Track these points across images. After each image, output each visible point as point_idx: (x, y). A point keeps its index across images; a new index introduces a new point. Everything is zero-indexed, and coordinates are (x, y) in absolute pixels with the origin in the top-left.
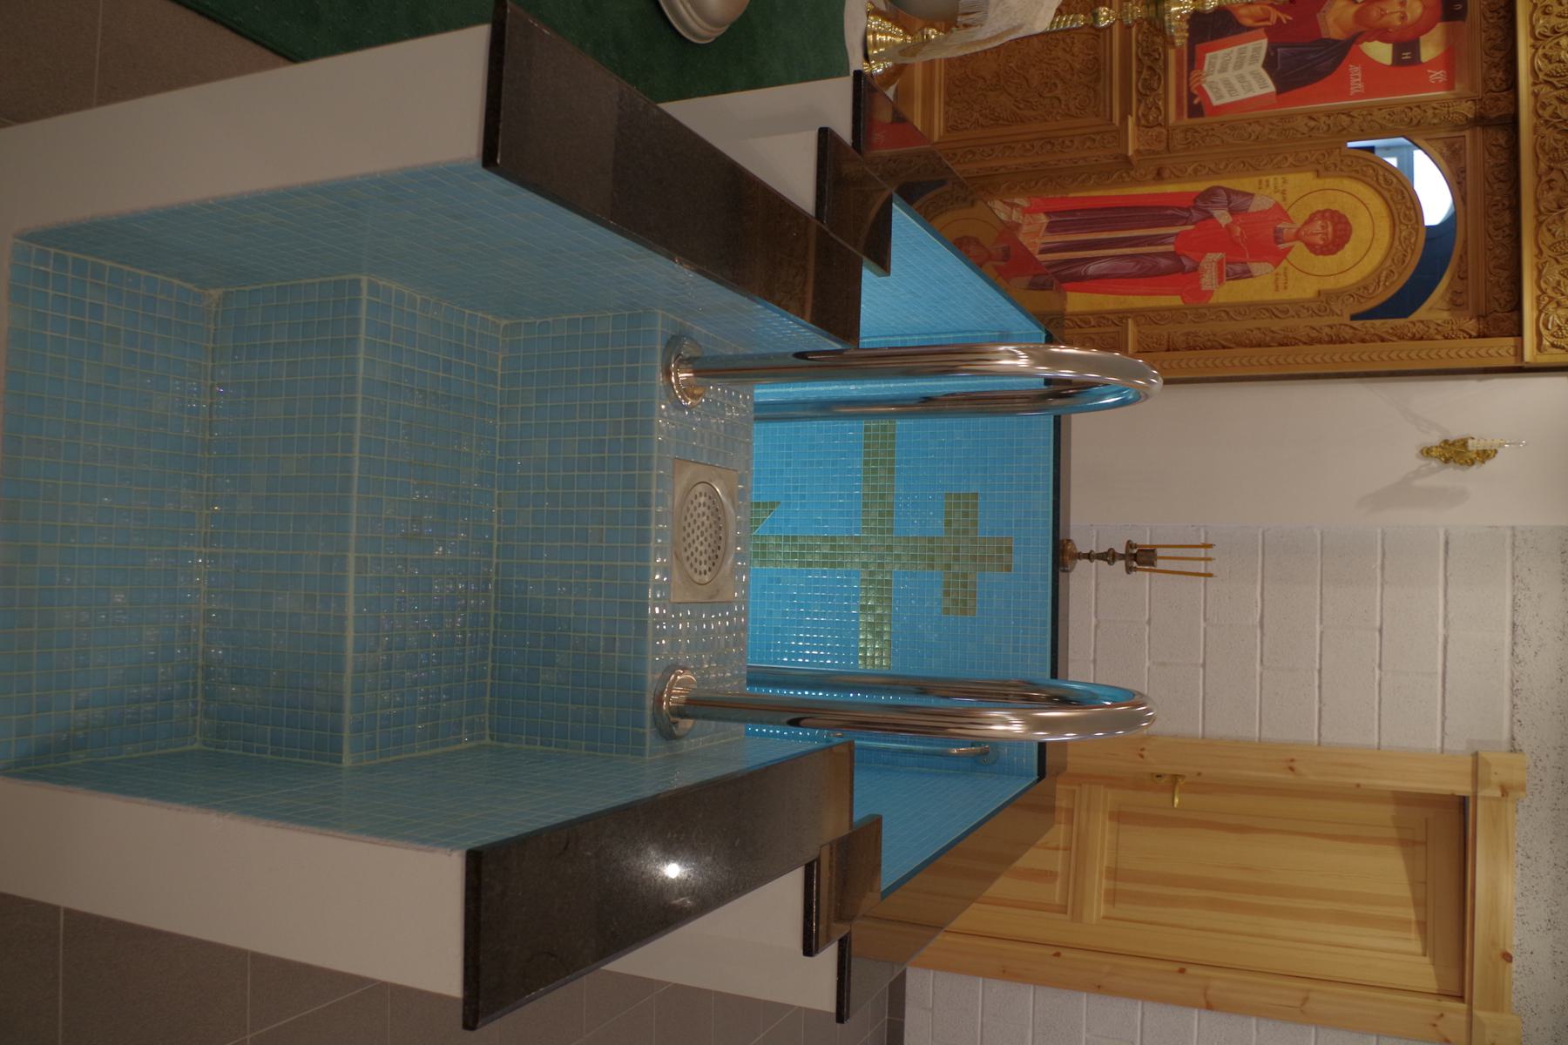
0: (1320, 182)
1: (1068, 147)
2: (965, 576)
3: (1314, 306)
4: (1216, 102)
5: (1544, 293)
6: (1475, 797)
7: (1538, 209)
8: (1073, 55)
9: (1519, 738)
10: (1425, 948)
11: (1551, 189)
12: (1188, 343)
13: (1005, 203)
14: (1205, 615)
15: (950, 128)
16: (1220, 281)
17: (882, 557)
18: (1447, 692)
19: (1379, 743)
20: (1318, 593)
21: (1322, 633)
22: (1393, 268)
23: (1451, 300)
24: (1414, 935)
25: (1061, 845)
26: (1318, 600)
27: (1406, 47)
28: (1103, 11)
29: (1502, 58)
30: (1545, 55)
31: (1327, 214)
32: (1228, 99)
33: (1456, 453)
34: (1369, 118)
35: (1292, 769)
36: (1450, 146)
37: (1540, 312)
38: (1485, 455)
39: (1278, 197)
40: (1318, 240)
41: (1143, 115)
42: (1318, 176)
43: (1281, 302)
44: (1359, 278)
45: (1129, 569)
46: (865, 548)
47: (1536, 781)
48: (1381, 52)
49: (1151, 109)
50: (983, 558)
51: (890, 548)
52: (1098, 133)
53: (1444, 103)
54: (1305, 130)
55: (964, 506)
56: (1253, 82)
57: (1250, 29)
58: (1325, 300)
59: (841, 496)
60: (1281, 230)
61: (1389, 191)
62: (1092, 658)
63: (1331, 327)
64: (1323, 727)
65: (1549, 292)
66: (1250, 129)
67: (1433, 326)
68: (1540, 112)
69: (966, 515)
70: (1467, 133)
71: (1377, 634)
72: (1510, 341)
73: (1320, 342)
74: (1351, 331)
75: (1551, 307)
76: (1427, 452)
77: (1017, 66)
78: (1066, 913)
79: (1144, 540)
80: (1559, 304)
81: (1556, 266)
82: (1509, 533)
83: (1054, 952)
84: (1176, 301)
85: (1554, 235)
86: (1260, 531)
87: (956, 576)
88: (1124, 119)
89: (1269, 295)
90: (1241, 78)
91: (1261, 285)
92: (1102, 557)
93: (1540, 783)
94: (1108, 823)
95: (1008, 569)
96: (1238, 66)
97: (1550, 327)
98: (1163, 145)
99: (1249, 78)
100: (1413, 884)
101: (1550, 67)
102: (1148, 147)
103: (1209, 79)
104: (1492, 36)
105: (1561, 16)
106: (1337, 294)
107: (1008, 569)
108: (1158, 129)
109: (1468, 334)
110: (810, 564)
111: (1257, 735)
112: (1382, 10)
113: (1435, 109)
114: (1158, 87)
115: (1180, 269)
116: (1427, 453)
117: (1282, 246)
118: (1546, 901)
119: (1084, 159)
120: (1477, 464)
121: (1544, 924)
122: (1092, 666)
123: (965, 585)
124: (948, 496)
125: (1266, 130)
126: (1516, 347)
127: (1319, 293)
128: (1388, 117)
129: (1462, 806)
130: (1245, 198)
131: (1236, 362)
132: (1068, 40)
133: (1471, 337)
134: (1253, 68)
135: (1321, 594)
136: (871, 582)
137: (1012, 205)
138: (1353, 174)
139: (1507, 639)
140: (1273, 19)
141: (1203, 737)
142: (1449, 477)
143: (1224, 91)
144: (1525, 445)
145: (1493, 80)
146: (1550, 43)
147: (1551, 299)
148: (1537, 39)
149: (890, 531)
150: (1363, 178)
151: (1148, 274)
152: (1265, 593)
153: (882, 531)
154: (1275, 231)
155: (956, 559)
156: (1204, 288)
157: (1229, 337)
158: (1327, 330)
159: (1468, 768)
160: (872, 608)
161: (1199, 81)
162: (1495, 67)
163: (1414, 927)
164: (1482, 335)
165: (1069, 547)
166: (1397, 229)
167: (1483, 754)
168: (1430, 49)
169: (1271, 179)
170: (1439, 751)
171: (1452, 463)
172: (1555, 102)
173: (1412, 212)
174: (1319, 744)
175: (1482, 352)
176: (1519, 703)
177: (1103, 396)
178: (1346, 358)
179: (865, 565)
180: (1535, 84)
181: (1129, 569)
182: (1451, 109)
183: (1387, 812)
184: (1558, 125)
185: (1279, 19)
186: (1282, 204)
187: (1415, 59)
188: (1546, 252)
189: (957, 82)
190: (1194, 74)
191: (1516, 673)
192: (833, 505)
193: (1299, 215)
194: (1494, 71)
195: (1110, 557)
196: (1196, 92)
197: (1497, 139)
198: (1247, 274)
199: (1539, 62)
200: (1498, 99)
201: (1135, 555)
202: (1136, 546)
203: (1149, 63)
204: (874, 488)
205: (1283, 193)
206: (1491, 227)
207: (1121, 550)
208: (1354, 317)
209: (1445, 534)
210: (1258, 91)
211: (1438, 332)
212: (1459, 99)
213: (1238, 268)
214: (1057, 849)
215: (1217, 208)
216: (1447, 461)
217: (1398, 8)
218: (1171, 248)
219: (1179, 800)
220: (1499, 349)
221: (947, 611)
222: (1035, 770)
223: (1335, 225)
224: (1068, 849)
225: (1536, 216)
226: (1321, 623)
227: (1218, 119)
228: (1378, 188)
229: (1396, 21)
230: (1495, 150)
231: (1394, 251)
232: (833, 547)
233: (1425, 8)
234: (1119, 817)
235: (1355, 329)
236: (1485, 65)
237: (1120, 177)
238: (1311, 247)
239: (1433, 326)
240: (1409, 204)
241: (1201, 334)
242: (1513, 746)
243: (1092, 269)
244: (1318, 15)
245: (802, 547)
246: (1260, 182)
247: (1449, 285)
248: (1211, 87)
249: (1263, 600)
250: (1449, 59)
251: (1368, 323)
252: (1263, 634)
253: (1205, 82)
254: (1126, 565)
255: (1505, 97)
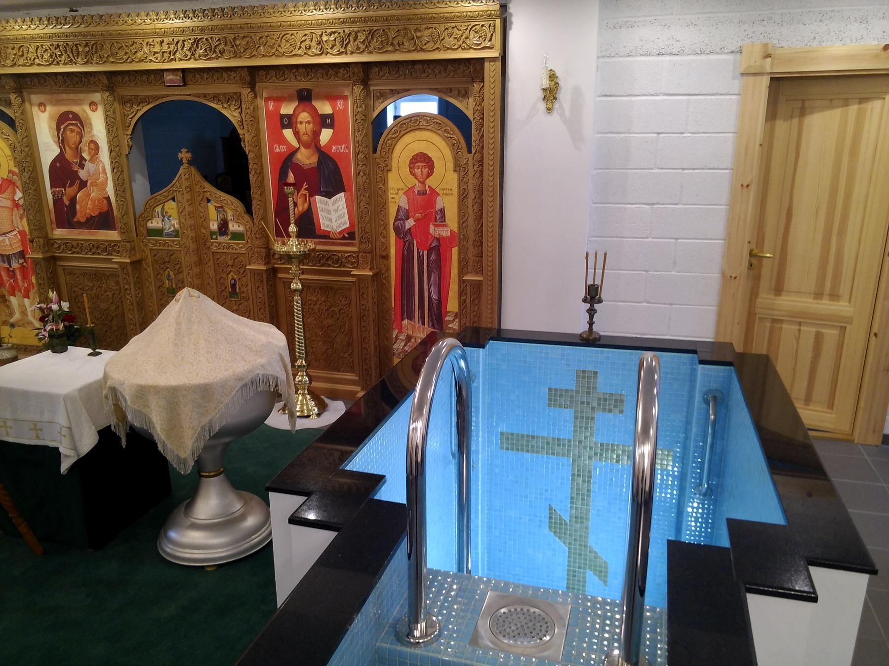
0: (393, 169)
1: (366, 307)
2: (599, 399)
3: (462, 174)
4: (348, 225)
5: (460, 46)
6: (771, 73)
7: (414, 50)
8: (318, 300)
9: (733, 49)
10: (878, 98)
11: (403, 44)
12: (479, 245)
13: (395, 343)
14: (644, 238)
15: (352, 370)
16: (445, 226)
17: (585, 448)
18: (700, 93)
19: (733, 133)
20: (633, 171)
21: (659, 168)
22: (443, 130)
23: (462, 97)
24: (869, 106)
25: (797, 327)
26: (638, 171)
27: (325, 121)
28: (293, 286)
29: (333, 70)
30: (331, 48)
31: (412, 166)
32: (346, 218)
33: (551, 94)
34: (360, 143)
35: (748, 186)
36: (378, 98)
37: (471, 48)
38: (552, 76)
39: (401, 193)
41: (352, 265)
42: (390, 170)
43: (459, 192)
44: (448, 148)
45: (600, 301)
46: (579, 457)
47: (762, 36)
48: (326, 135)
49: (349, 261)
50: (588, 388)
51: (580, 442)
52: (359, 291)
53: (354, 102)
54: (365, 178)
55: (556, 397)
56: (338, 204)
57: (310, 205)
58: (459, 167)
59: (547, 467)
60: (419, 191)
61: (401, 131)
62: (669, 306)
63: (474, 165)
64: (721, 167)
65: (460, 43)
66: (362, 208)
67: (477, 108)
68: (361, 50)
69: (561, 395)
70: (372, 88)
71: (661, 135)
72: (486, 64)
73: (482, 172)
74: (477, 154)
75: (468, 42)
76: (549, 110)
77: (321, 331)
78: (846, 327)
79: (582, 293)
80: (467, 38)
81: (446, 40)
82: (601, 60)
83: (874, 338)
84: (455, 251)
85: (428, 42)
86: (593, 205)
87: (599, 405)
88: (353, 276)
89: (455, 199)
90: (336, 211)
91: (449, 203)
92: (591, 317)
93: (763, 34)
94: (782, 298)
95: (596, 373)
96: (329, 212)
97: (480, 42)
98: (368, 255)
99: (336, 206)
100: (831, 107)
101: (337, 45)
102: (369, 264)
103: (335, 228)
104: (321, 75)
105: (312, 40)
106: (456, 160)
107: (596, 373)
108: (360, 257)
109: (482, 88)
110: (589, 491)
111: (724, 207)
112: (304, 134)
113: (357, 107)
114: (337, 256)
115: (437, 248)
116: (550, 110)
118: (846, 25)
119: (373, 298)
120: (558, 81)
121: (863, 25)
122: (674, 306)
123: (605, 400)
124: (549, 405)
125: (364, 199)
126: (490, 61)
127: (455, 171)
128: (360, 132)
129: (777, 82)
130: (401, 211)
131: (491, 220)
132: (310, 302)
133: (483, 86)
134: (331, 205)
135: (634, 169)
136: (601, 455)
137: (397, 338)
138: (391, 150)
139: (667, 58)
140: (306, 192)
141: (725, 240)
142: (565, 96)
143: (341, 220)
144: (547, 55)
145: (344, 75)
146: (326, 46)
147: (464, 42)
148: (323, 52)
149: (569, 441)
150: (393, 146)
151: (439, 265)
152: (631, 202)
153: (570, 446)
154: (419, 195)
155: (588, 403)
156: (449, 234)
157: (476, 222)
158: (476, 167)
159: (751, 78)
160: (618, 456)
161: (336, 234)
162: (337, 74)
163: (863, 106)
164: (483, 81)
165: (585, 336)
166: (421, 127)
167: (742, 72)
168: (325, 108)
169: (390, 196)
170: (739, 97)
171: (557, 96)
172: (356, 43)
173: (413, 119)
174: (732, 169)
175: (492, 80)
176: (708, 50)
177: (460, 368)
178: (491, 158)
179: (590, 458)
180: (346, 53)
182: (358, 98)
183: (781, 126)
184: (369, 41)
185: (306, 189)
186: (404, 191)
187: (331, 116)
188: (437, 46)
189: (328, 364)
190: (332, 236)
191: (690, 52)
192: (552, 473)
193: (412, 181)
194: (339, 75)
195: (591, 312)
196: (341, 236)
197: (376, 73)
198: (442, 211)
199: (335, 51)
200: (354, 73)
201: (591, 297)
202: (586, 297)
203: (325, 260)
204: (543, 448)
205: (398, 190)
206: (423, 75)
207: (588, 306)
208: (470, 152)
209: (600, 97)
210: (343, 202)
211: (480, 104)
212: (352, 93)
213: (439, 216)
214: (799, 330)
215: (405, 226)
216: (555, 98)
217: (303, 125)
218: (426, 252)
219: (767, 253)
220: (491, 71)
221: (621, 412)
222: (728, 368)
223: (417, 162)
224: (800, 324)
225: (418, 52)
226: (652, 169)
227: (356, 224)
228: (399, 137)
230: (381, 74)
231: (434, 129)
232: (579, 476)
233: (304, 111)
234: (778, 290)
235: (476, 151)
236: (336, 79)
237: (385, 278)
238: (429, 175)
239: (477, 108)
240: (408, 121)
241: (474, 239)
242: (738, 52)
243: (434, 296)
244: (305, 168)
245: (577, 494)
246: (392, 202)
248: (340, 227)
249: (636, 204)
250: (331, 98)
251: (473, 144)
252: (658, 204)
253: (336, 230)
254: (597, 303)
255: (352, 69)
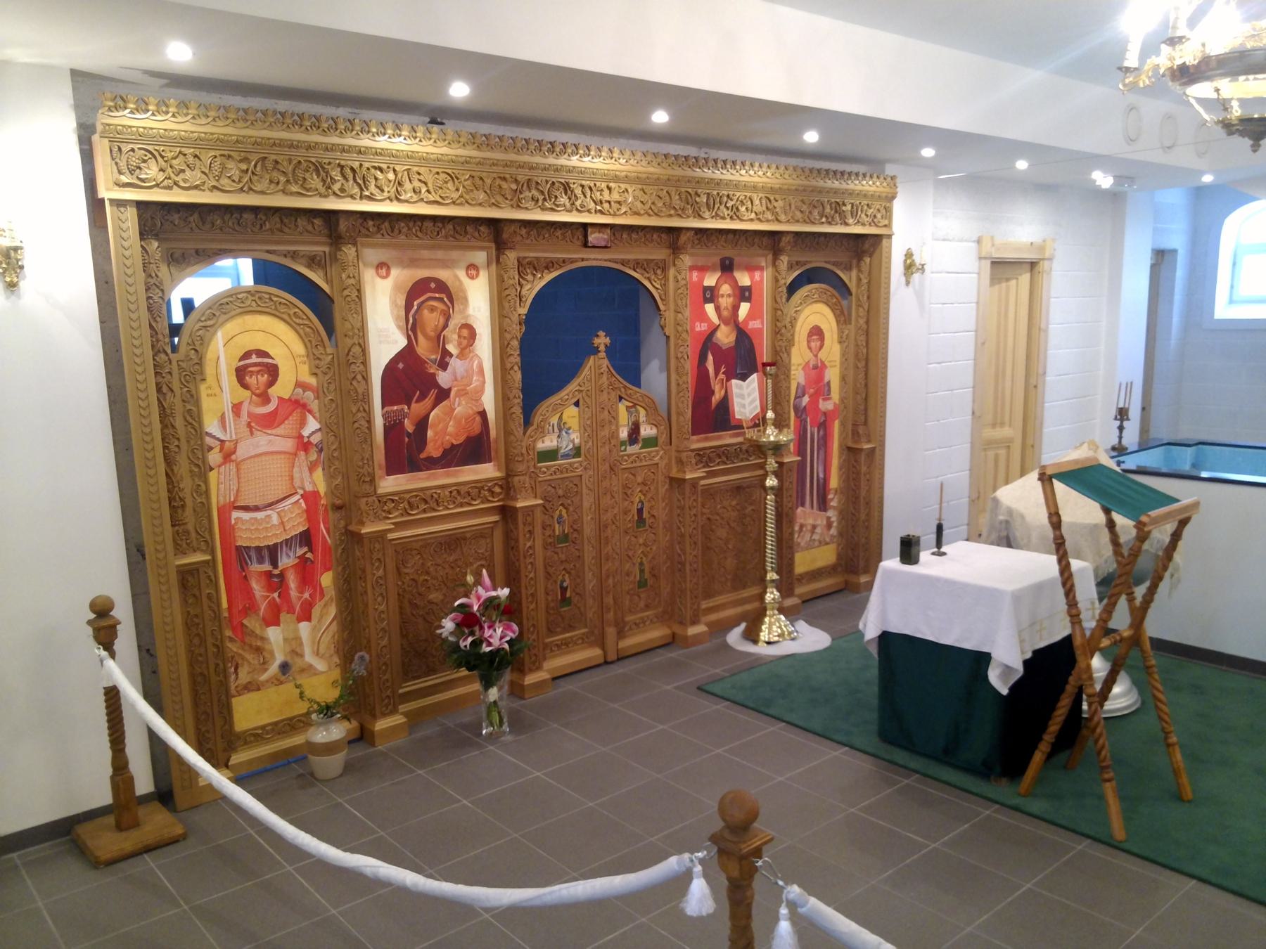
10: (1013, 278)
39: (800, 368)
40: (818, 343)
45: (1128, 419)
48: (744, 308)
76: (908, 283)
79: (1114, 412)
91: (833, 376)
103: (748, 415)
117: (819, 365)
129: (997, 264)
154: (813, 369)
181: (1128, 419)
185: (723, 373)
187: (749, 289)
195: (1121, 428)
198: (829, 383)
229: (730, 300)
243: (821, 475)
247: (841, 270)
250: (750, 269)
